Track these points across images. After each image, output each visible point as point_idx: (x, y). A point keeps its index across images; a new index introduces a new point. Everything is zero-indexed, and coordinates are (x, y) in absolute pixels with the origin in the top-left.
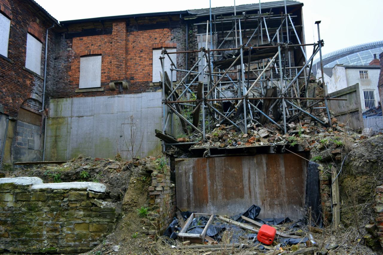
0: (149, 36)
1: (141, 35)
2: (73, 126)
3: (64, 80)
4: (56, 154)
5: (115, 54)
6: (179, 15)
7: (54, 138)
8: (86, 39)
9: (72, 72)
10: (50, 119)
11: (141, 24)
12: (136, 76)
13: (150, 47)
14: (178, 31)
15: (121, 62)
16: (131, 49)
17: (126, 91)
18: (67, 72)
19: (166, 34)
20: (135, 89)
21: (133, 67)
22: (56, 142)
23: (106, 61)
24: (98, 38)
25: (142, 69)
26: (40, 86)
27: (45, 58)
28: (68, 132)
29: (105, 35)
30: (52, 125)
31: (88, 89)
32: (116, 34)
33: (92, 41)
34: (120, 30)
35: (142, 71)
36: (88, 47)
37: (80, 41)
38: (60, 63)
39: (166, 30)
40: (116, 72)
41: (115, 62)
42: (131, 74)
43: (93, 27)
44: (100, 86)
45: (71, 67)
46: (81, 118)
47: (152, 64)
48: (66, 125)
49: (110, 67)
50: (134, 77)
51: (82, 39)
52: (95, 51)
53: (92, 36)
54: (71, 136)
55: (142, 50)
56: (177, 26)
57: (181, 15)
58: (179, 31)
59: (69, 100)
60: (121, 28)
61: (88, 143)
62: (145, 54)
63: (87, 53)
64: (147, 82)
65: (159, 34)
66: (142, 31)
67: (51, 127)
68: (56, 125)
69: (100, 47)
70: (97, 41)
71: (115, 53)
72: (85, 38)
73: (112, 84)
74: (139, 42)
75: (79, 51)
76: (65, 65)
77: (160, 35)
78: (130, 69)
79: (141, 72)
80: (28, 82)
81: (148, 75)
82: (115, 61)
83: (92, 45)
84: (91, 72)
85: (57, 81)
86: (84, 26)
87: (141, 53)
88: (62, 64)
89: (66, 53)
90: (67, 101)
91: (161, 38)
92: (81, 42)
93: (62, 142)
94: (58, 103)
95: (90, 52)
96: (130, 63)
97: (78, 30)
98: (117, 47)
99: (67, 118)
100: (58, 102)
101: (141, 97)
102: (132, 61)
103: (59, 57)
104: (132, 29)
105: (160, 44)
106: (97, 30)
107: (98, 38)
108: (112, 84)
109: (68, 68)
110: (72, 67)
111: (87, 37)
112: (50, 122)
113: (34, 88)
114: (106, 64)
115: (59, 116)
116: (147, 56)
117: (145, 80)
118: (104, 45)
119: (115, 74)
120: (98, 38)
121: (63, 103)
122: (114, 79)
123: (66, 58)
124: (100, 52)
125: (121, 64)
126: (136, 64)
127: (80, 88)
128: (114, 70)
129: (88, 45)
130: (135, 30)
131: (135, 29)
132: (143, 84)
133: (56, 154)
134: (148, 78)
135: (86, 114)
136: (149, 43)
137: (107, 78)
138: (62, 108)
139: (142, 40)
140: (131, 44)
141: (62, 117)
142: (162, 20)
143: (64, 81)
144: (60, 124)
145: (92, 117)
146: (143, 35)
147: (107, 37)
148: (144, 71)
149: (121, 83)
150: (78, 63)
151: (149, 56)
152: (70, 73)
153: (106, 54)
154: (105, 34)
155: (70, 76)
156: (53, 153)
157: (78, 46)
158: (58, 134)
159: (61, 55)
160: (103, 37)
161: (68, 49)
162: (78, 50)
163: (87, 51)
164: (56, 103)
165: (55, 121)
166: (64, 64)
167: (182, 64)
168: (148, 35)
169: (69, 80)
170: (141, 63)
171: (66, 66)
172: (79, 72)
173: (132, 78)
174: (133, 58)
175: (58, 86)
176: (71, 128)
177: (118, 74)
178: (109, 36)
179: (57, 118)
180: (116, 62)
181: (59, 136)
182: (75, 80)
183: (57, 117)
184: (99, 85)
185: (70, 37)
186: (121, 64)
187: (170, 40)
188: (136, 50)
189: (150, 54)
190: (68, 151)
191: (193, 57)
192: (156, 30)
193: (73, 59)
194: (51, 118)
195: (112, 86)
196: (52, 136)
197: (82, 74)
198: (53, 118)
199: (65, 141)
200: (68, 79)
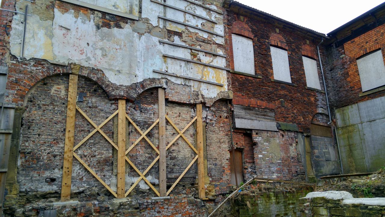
3: (344, 88)
9: (351, 78)
10: (340, 129)
22: (351, 151)
24: (372, 33)
26: (323, 100)
28: (362, 140)
29: (380, 27)
36: (363, 46)
37: (352, 44)
38: (336, 72)
43: (364, 24)
45: (348, 73)
46: (373, 122)
48: (358, 132)
51: (354, 41)
52: (371, 47)
59: (355, 106)
67: (342, 136)
69: (377, 41)
72: (356, 39)
75: (353, 54)
76: (342, 73)
80: (312, 99)
83: (367, 43)
85: (337, 91)
86: (353, 27)
88: (338, 73)
89: (340, 61)
90: (352, 107)
92: (353, 44)
93: (358, 150)
94: (344, 112)
95: (366, 50)
100: (343, 111)
103: (334, 67)
106: (368, 26)
111: (359, 37)
112: (340, 131)
113: (319, 103)
115: (348, 124)
118: (382, 37)
121: (349, 110)
123: (341, 66)
124: (377, 46)
127: (363, 91)
135: (378, 117)
138: (349, 116)
144: (351, 132)
147: (382, 27)
152: (349, 79)
158: (351, 143)
159: (335, 64)
160: (377, 29)
161: (341, 57)
163: (362, 51)
165: (344, 130)
166: (341, 72)
169: (349, 87)
172: (359, 75)
179: (346, 127)
183: (345, 125)
185: (341, 44)
193: (349, 64)
194: (340, 128)
198: (342, 128)
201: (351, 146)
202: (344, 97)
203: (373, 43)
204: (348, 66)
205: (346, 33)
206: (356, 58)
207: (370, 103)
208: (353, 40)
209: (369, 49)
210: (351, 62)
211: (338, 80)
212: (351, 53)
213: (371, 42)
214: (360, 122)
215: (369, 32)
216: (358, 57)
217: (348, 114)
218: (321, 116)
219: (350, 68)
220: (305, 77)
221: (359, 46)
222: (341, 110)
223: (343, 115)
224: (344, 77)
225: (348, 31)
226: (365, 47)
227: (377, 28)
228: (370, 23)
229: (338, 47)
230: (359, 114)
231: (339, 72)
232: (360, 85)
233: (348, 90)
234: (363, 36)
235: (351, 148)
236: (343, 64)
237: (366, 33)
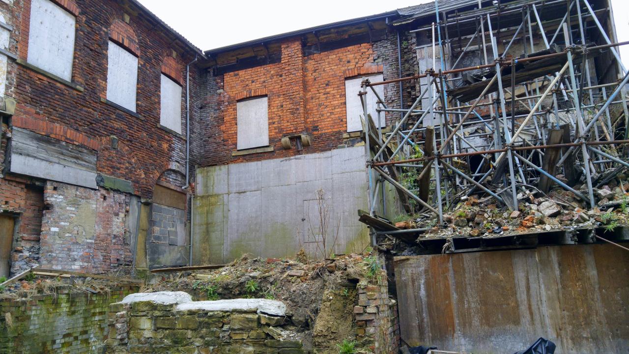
11: (325, 41)
12: (321, 125)
13: (340, 76)
17: (307, 148)
20: (320, 145)
22: (208, 232)
24: (260, 70)
26: (181, 151)
28: (225, 217)
29: (271, 65)
38: (208, 113)
43: (253, 55)
44: (268, 145)
46: (242, 194)
47: (345, 103)
48: (222, 206)
51: (238, 75)
54: (229, 223)
55: (329, 81)
59: (224, 168)
60: (292, 52)
61: (254, 233)
64: (340, 133)
66: (326, 53)
67: (200, 210)
69: (264, 84)
72: (241, 73)
73: (285, 140)
77: (356, 55)
78: (312, 114)
80: (165, 146)
82: (288, 103)
83: (253, 82)
85: (204, 141)
86: (239, 54)
88: (211, 115)
89: (216, 98)
91: (357, 60)
92: (236, 78)
95: (250, 92)
100: (207, 172)
101: (331, 157)
103: (206, 104)
109: (221, 120)
111: (244, 70)
113: (174, 154)
114: (275, 110)
115: (210, 193)
119: (289, 124)
122: (288, 132)
125: (298, 107)
127: (238, 149)
138: (214, 181)
140: (310, 75)
143: (215, 141)
149: (299, 137)
151: (340, 91)
152: (223, 127)
158: (210, 221)
159: (208, 101)
160: (268, 67)
161: (219, 91)
165: (204, 201)
168: (336, 57)
170: (329, 104)
171: (217, 117)
172: (236, 124)
173: (316, 128)
178: (278, 66)
179: (208, 196)
185: (220, 73)
186: (298, 107)
187: (372, 61)
188: (319, 84)
195: (286, 142)
198: (202, 197)
199: (221, 231)
210: (229, 103)
211: (208, 125)
222: (205, 171)
223: (207, 179)
225: (233, 56)
233: (219, 143)
235: (208, 227)
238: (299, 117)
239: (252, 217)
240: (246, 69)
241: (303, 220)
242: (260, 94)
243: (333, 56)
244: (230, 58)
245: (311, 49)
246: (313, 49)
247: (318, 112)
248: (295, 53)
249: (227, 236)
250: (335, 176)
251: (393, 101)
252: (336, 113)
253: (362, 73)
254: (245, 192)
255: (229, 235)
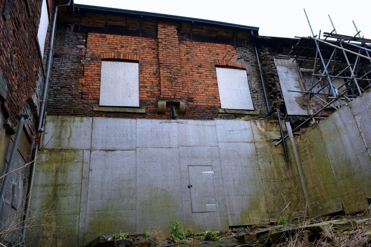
0: (208, 49)
1: (196, 46)
2: (93, 166)
3: (70, 90)
4: (54, 223)
5: (165, 62)
6: (250, 31)
7: (51, 188)
8: (113, 37)
9: (86, 80)
10: (45, 151)
11: (197, 33)
12: (197, 98)
13: (211, 63)
14: (245, 51)
15: (176, 74)
16: (185, 61)
17: (183, 115)
18: (75, 79)
19: (230, 51)
20: (196, 115)
21: (190, 85)
22: (55, 196)
23: (147, 71)
24: (132, 40)
25: (205, 89)
27: (49, 46)
28: (85, 178)
29: (143, 38)
30: (47, 162)
31: (117, 108)
32: (164, 37)
33: (122, 42)
34: (170, 34)
35: (205, 91)
36: (115, 48)
37: (101, 39)
38: (64, 63)
39: (229, 47)
40: (168, 87)
41: (165, 74)
42: (188, 93)
43: (124, 25)
44: (138, 106)
45: (84, 72)
46: (110, 152)
47: (217, 84)
48: (80, 165)
49: (154, 81)
50: (193, 98)
51: (105, 37)
52: (127, 55)
53: (122, 35)
54: (90, 185)
55: (201, 64)
56: (243, 45)
57: (252, 31)
58: (246, 51)
59: (87, 121)
61: (126, 200)
62: (206, 70)
63: (114, 57)
65: (222, 50)
66: (197, 43)
67: (46, 166)
68: (57, 163)
69: (135, 51)
70: (131, 43)
71: (164, 61)
72: (109, 36)
73: (162, 104)
74: (195, 54)
75: (99, 51)
76: (73, 67)
77: (223, 51)
78: (186, 87)
79: (203, 92)
81: (213, 97)
82: (166, 71)
83: (122, 47)
84: (120, 82)
85: (55, 90)
86: (110, 20)
87: (200, 68)
89: (75, 52)
90: (81, 121)
91: (224, 55)
92: (102, 40)
93: (71, 197)
94: (64, 124)
95: (119, 55)
96: (185, 78)
97: (98, 24)
98: (167, 54)
99: (81, 152)
100: (63, 121)
101: (215, 126)
102: (188, 76)
103: (63, 54)
104: (184, 37)
105: (224, 61)
106: (129, 29)
107: (132, 40)
108: (162, 104)
110: (85, 72)
111: (113, 35)
112: (44, 157)
114: (147, 76)
115: (65, 145)
116: (209, 73)
117: (210, 105)
118: (142, 50)
119: (167, 89)
120: (132, 40)
121: (75, 124)
122: (166, 96)
123: (75, 58)
124: (135, 57)
125: (176, 76)
126: (194, 81)
127: (101, 104)
128: (164, 83)
129: (116, 46)
130: (187, 39)
131: (188, 38)
132: (208, 109)
133: (54, 223)
134: (214, 102)
135: (119, 146)
136: (211, 59)
137: (149, 94)
138: (71, 132)
139: (199, 53)
140: (183, 55)
141: (72, 150)
142: (224, 34)
143: (70, 92)
144: (66, 162)
145: (133, 151)
146: (199, 47)
147: (146, 40)
148: (207, 93)
150: (97, 68)
151: (212, 74)
152: (82, 80)
153: (145, 62)
154: (142, 36)
155: (83, 85)
156: (47, 220)
157: (97, 45)
158: (60, 181)
159: (65, 52)
160: (140, 39)
161: (79, 46)
162: (98, 50)
163: (113, 54)
164: (59, 124)
165: (54, 156)
166: (72, 65)
167: (257, 90)
168: (206, 48)
169: (80, 91)
170: (202, 82)
171: (75, 69)
172: (100, 80)
174: (189, 73)
175: (58, 97)
176: (90, 170)
177: (172, 90)
178: (150, 41)
179: (60, 150)
180: (167, 74)
181: (63, 185)
182: (92, 92)
183: (59, 148)
184: (136, 104)
185: (85, 31)
186: (176, 76)
187: (237, 59)
188: (192, 64)
189: (213, 72)
190: (82, 214)
191: (272, 83)
192: (217, 44)
193: (89, 61)
194: (47, 149)
195: (163, 106)
196: (46, 185)
197: (104, 84)
198: (51, 151)
199: (77, 195)
200: (78, 89)
201: (59, 188)
202: (65, 103)
203: (130, 51)
204: (87, 63)
205: (97, 22)
206: (102, 58)
207: (112, 122)
208: (104, 35)
209: (124, 56)
210: (92, 59)
211: (62, 74)
212: (97, 49)
213: (128, 49)
214: (89, 147)
215: (129, 37)
216: (105, 57)
217: (71, 130)
218: (30, 112)
219: (89, 66)
220: (38, 28)
221: (111, 46)
222: (59, 120)
223: (61, 129)
224: (76, 75)
225: (102, 20)
226: (119, 50)
227: (139, 38)
228: (132, 28)
229: (78, 32)
230: (90, 135)
231: (69, 64)
232: (98, 94)
233: (75, 95)
234: (119, 37)
235: (56, 191)
236: (79, 58)
237: (124, 36)
238: (177, 85)
239: (123, 180)
240: (115, 34)
241: (189, 187)
242: (130, 59)
243: (204, 47)
244: (98, 21)
245: (183, 36)
246: (185, 36)
247: (192, 86)
248: (172, 34)
249: (86, 202)
250: (221, 145)
251: (256, 91)
252: (210, 91)
253: (229, 65)
254: (111, 150)
255: (89, 201)
